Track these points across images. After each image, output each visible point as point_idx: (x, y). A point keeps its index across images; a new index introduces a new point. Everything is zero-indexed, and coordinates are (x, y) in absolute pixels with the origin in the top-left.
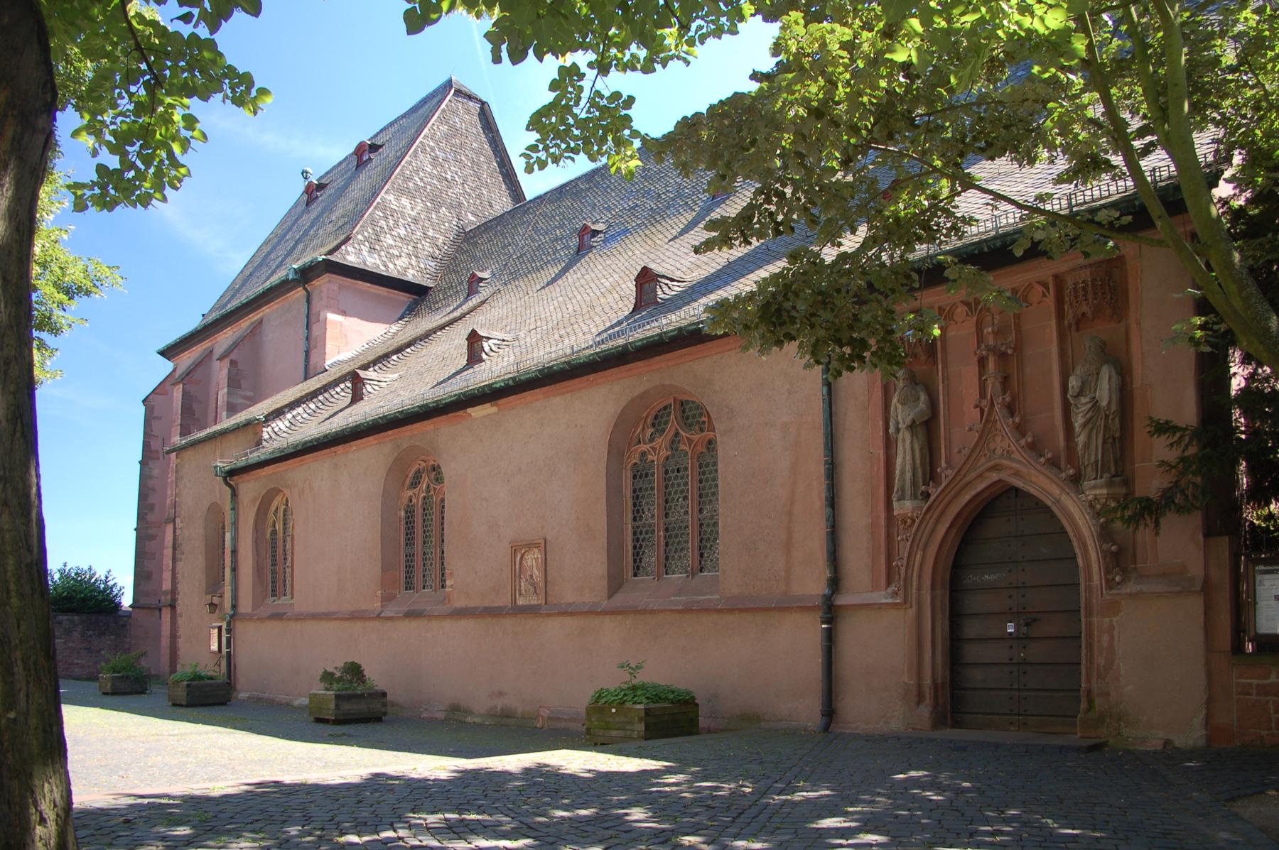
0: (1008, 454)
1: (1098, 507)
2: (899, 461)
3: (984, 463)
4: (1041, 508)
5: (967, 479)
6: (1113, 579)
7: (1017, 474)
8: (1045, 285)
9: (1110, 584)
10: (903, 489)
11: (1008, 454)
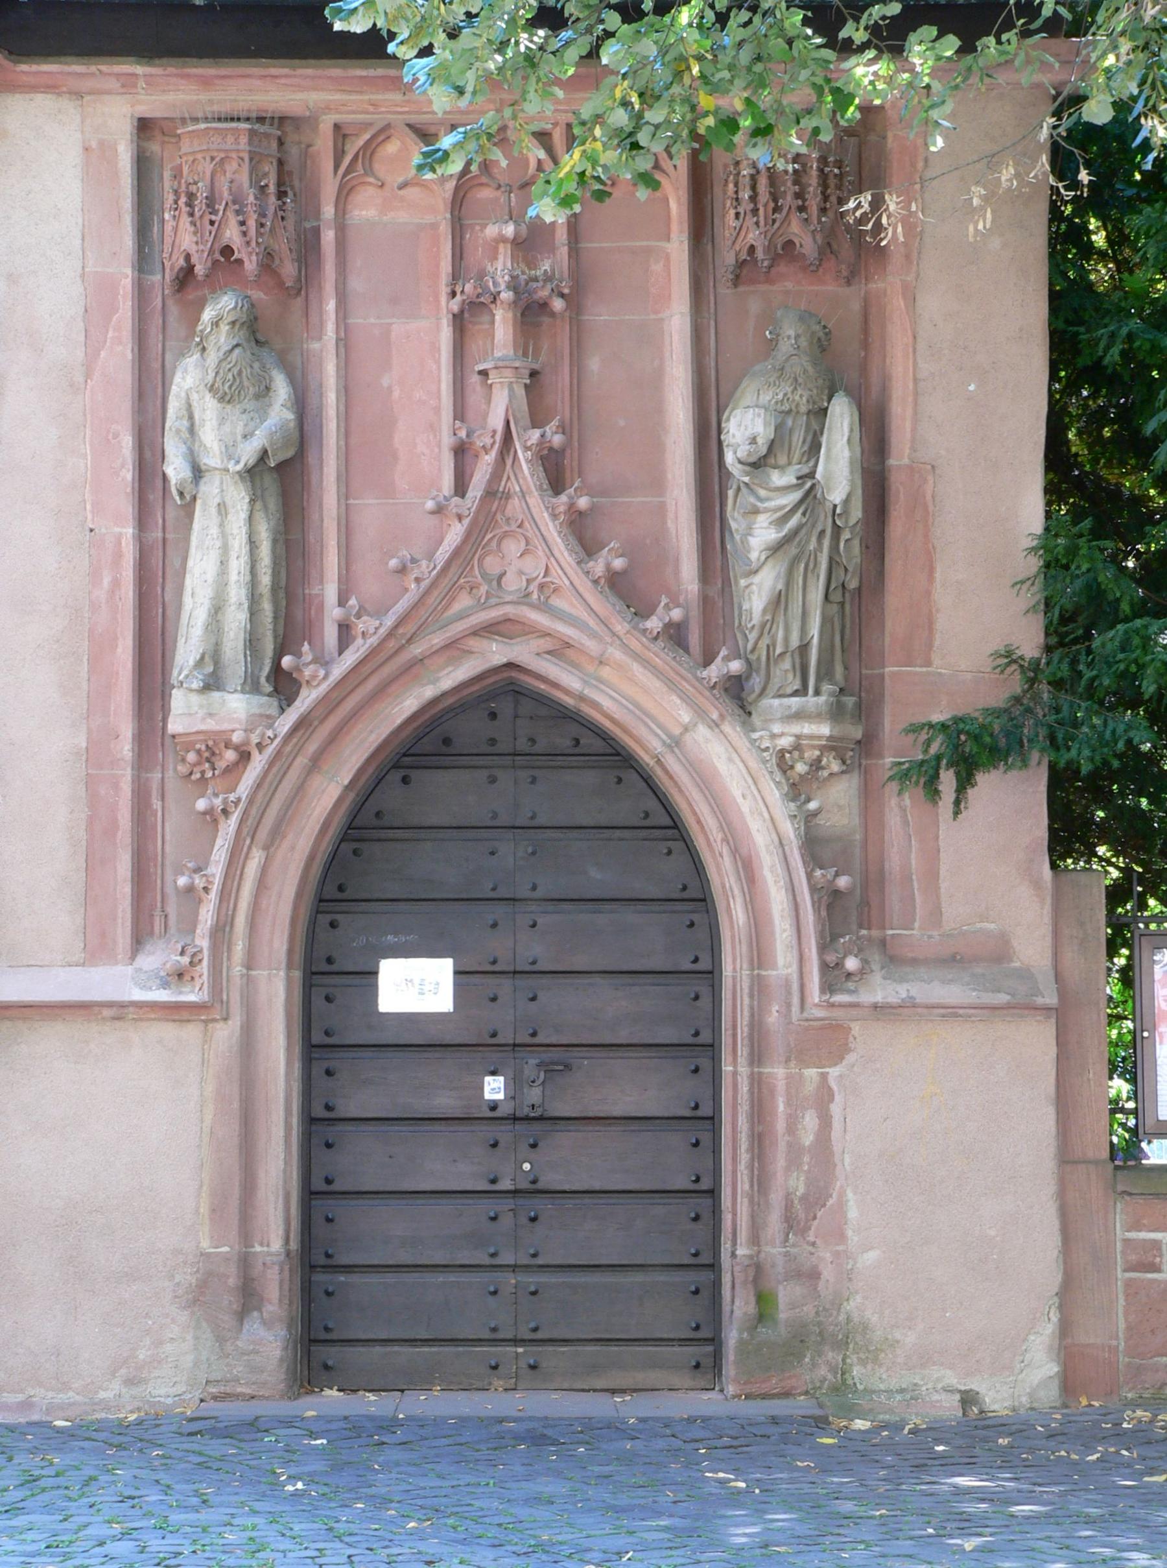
0: (543, 592)
4: (611, 757)
5: (417, 650)
6: (839, 965)
7: (561, 650)
9: (834, 976)
10: (213, 658)
11: (543, 592)
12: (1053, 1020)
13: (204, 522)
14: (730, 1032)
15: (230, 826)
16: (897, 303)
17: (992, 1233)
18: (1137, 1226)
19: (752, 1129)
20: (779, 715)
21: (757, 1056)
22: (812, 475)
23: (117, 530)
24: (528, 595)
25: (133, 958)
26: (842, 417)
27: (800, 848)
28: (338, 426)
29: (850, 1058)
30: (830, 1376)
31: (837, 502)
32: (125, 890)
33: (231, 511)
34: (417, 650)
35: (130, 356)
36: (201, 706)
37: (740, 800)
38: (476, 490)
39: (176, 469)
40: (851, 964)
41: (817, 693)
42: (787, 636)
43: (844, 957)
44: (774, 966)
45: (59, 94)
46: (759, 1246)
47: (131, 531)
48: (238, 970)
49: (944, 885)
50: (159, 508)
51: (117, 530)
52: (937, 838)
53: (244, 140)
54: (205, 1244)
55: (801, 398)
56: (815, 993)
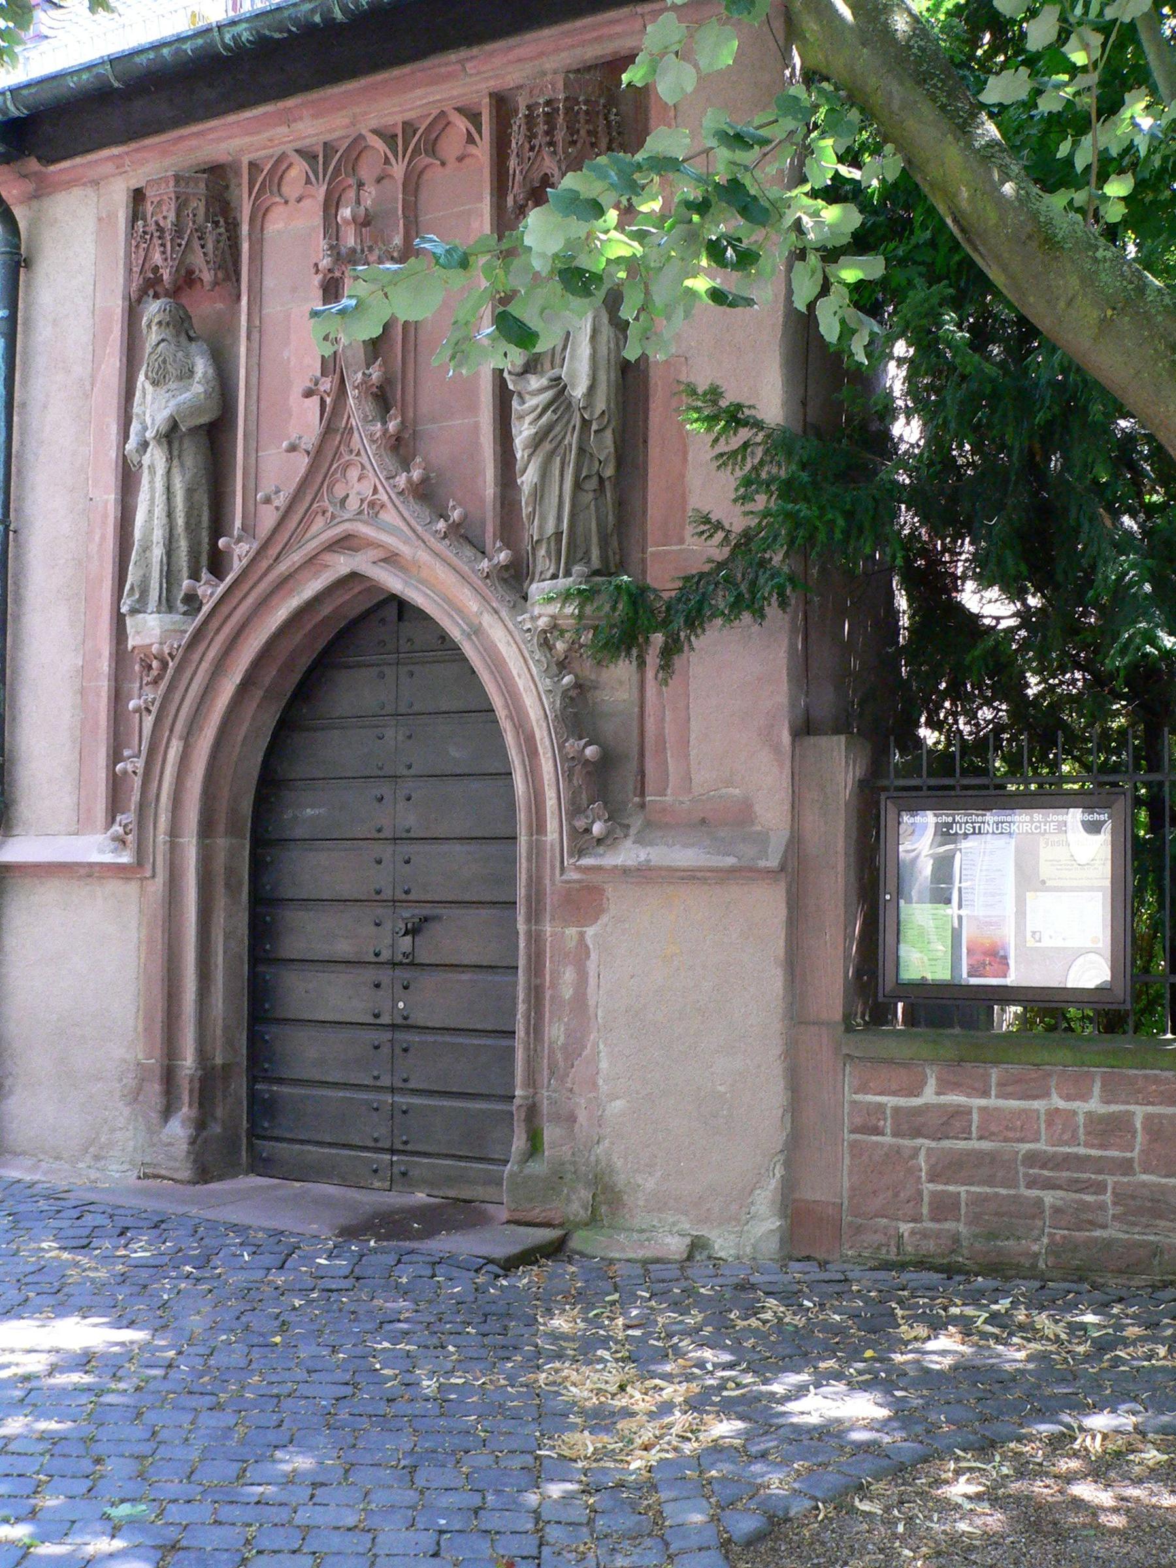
1: (560, 646)
3: (320, 532)
5: (283, 567)
6: (588, 831)
7: (391, 559)
12: (783, 885)
17: (722, 1089)
18: (863, 1089)
19: (529, 981)
21: (535, 914)
29: (604, 919)
30: (582, 1212)
34: (283, 567)
43: (593, 822)
46: (535, 1087)
47: (113, 496)
49: (693, 753)
53: (202, 185)
54: (140, 1056)
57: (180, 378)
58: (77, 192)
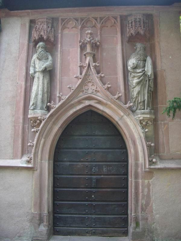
1: (144, 123)
2: (34, 88)
3: (82, 96)
5: (72, 102)
6: (152, 160)
7: (100, 102)
8: (116, 18)
9: (151, 163)
10: (35, 105)
13: (36, 80)
14: (130, 173)
15: (37, 134)
16: (157, 44)
20: (139, 114)
22: (144, 70)
23: (22, 83)
24: (93, 92)
25: (21, 158)
26: (149, 61)
27: (144, 138)
28: (60, 65)
29: (154, 178)
31: (149, 75)
32: (20, 146)
33: (40, 78)
34: (72, 102)
35: (26, 55)
36: (33, 112)
37: (132, 130)
38: (83, 74)
39: (31, 71)
40: (154, 160)
41: (147, 109)
42: (140, 99)
43: (153, 159)
44: (139, 161)
45: (18, 17)
47: (24, 83)
48: (39, 161)
49: (170, 145)
50: (29, 79)
51: (22, 83)
52: (169, 136)
54: (33, 211)
55: (142, 58)
56: (147, 166)
57: (45, 59)
58: (15, 18)
